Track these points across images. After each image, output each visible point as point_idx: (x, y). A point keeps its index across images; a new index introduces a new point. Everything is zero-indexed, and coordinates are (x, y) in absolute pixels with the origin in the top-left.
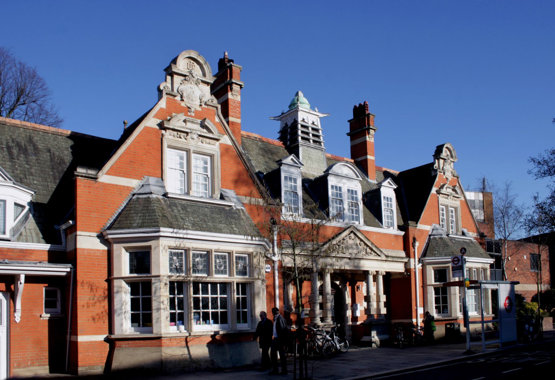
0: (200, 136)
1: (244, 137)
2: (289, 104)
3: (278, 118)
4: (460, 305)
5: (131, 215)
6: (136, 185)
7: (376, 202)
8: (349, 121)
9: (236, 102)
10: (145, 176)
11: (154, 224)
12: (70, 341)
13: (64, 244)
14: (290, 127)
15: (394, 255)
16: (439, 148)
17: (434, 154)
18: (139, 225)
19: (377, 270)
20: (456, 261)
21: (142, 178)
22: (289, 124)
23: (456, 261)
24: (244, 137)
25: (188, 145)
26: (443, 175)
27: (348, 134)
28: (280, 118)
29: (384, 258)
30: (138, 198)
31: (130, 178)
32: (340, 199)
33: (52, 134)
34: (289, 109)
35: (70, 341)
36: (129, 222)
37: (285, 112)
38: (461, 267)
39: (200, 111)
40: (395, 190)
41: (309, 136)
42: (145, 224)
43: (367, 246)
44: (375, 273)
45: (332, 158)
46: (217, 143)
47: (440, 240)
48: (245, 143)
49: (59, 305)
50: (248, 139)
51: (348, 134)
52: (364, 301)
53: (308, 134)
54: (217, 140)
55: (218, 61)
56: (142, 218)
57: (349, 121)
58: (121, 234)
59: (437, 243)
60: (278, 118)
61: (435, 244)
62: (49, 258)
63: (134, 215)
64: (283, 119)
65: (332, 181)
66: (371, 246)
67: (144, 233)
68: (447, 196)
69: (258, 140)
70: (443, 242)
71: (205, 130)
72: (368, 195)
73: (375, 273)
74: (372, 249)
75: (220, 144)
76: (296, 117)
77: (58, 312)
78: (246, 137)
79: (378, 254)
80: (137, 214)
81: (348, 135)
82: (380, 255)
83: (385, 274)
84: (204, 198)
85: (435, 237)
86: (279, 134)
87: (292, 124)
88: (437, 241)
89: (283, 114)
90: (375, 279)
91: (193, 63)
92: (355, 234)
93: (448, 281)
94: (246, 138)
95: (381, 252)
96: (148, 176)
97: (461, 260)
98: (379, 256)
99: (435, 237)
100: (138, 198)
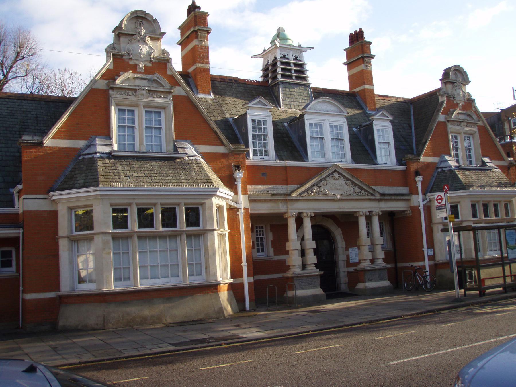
0: (149, 91)
1: (217, 81)
2: (271, 41)
3: (260, 56)
4: (478, 241)
5: (75, 176)
6: (83, 145)
7: (370, 136)
8: (345, 50)
9: (204, 48)
10: (92, 136)
11: (94, 184)
12: (23, 299)
13: (17, 206)
14: (271, 64)
15: (392, 192)
16: (446, 71)
17: (441, 78)
18: (81, 185)
19: (370, 210)
20: (439, 199)
21: (89, 138)
22: (270, 62)
23: (439, 199)
24: (217, 81)
25: (137, 101)
26: (453, 100)
27: (345, 64)
28: (262, 56)
29: (378, 197)
30: (84, 158)
31: (77, 139)
32: (321, 137)
33: (17, 99)
34: (270, 46)
35: (23, 299)
36: (72, 182)
37: (266, 49)
38: (444, 206)
39: (150, 67)
40: (391, 121)
41: (291, 73)
42: (87, 184)
43: (356, 185)
44: (368, 214)
45: (323, 92)
46: (170, 97)
47: (449, 173)
48: (218, 87)
49: (14, 263)
50: (222, 83)
51: (345, 64)
52: (505, 216)
53: (289, 70)
54: (171, 93)
55: (187, 8)
56: (84, 178)
57: (345, 50)
58: (65, 194)
59: (446, 176)
60: (260, 56)
61: (443, 177)
62: (30, 212)
63: (79, 175)
64: (265, 57)
65: (308, 120)
66: (360, 185)
67: (90, 192)
68: (458, 123)
69: (234, 81)
70: (453, 174)
71: (155, 85)
72: (361, 129)
73: (368, 214)
74: (362, 189)
75: (173, 96)
76: (275, 54)
77: (14, 271)
78: (219, 80)
79: (369, 193)
80: (81, 174)
81: (345, 65)
82: (374, 194)
83: (380, 213)
84: (151, 152)
85: (444, 169)
86: (261, 72)
87: (272, 61)
88: (446, 173)
89: (265, 51)
90: (369, 218)
91: (141, 21)
92: (339, 173)
93: (65, 287)
94: (219, 81)
95: (374, 190)
96: (95, 135)
97: (444, 199)
98: (372, 194)
99: (444, 169)
100: (84, 158)
